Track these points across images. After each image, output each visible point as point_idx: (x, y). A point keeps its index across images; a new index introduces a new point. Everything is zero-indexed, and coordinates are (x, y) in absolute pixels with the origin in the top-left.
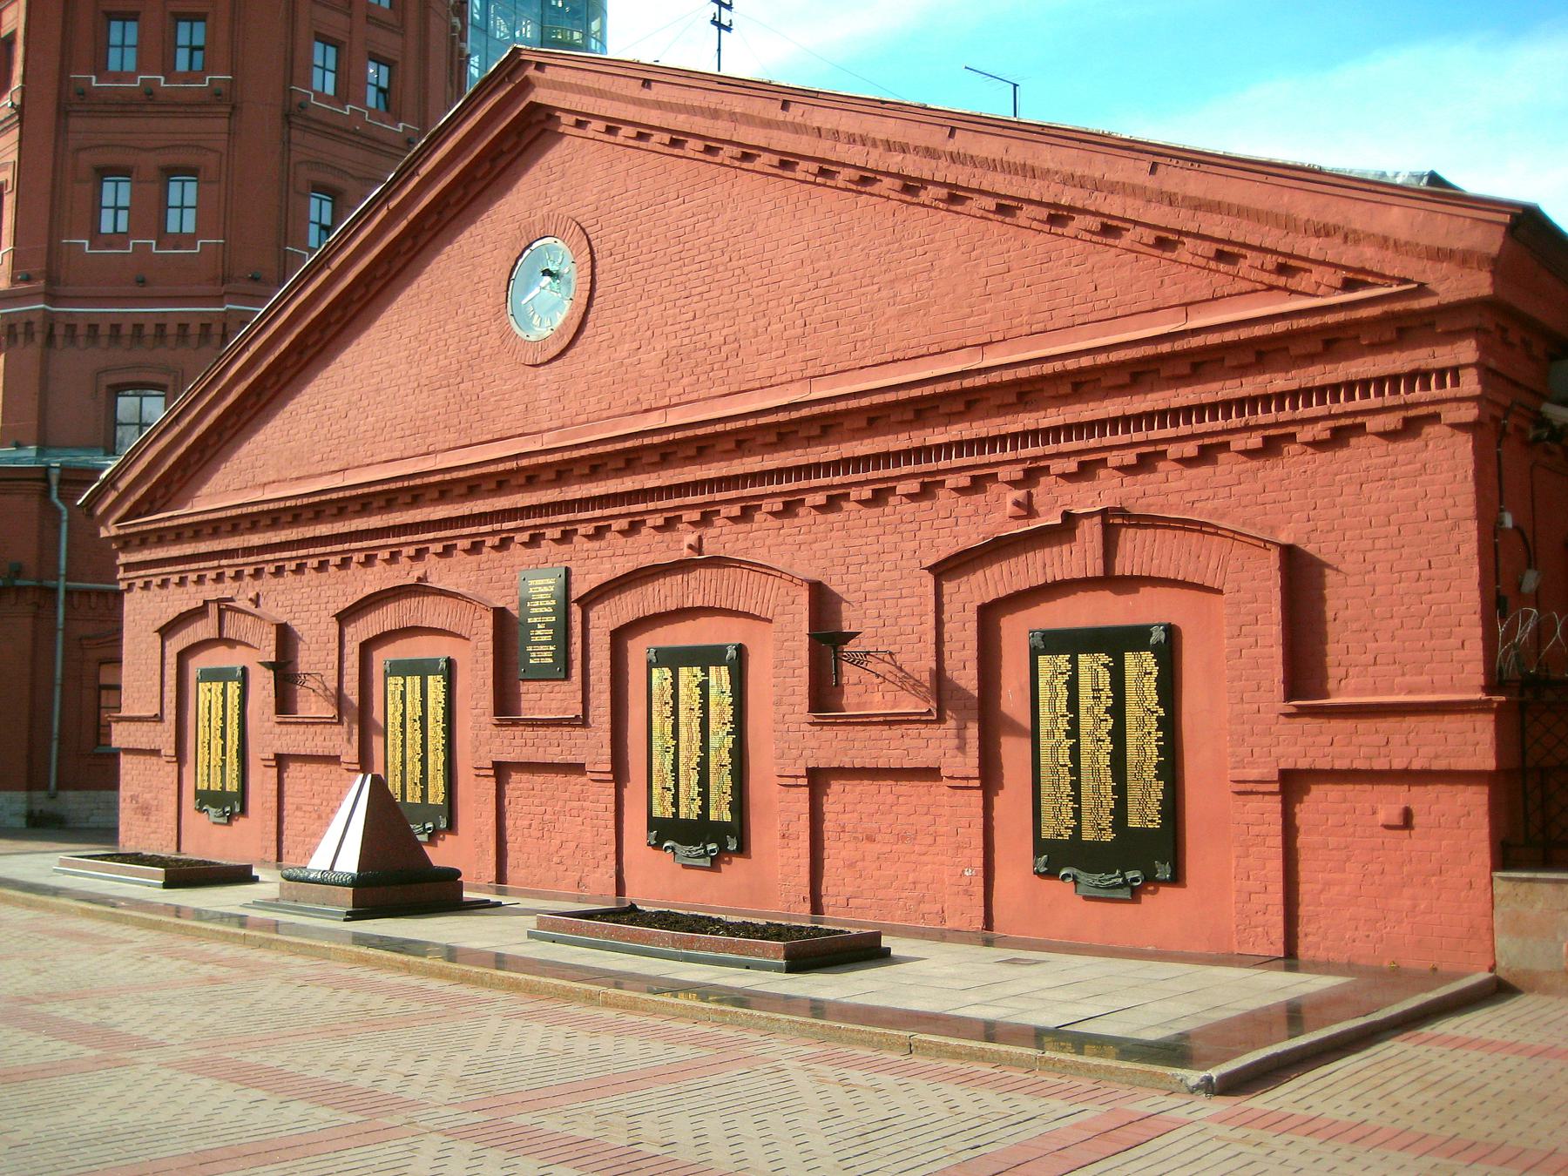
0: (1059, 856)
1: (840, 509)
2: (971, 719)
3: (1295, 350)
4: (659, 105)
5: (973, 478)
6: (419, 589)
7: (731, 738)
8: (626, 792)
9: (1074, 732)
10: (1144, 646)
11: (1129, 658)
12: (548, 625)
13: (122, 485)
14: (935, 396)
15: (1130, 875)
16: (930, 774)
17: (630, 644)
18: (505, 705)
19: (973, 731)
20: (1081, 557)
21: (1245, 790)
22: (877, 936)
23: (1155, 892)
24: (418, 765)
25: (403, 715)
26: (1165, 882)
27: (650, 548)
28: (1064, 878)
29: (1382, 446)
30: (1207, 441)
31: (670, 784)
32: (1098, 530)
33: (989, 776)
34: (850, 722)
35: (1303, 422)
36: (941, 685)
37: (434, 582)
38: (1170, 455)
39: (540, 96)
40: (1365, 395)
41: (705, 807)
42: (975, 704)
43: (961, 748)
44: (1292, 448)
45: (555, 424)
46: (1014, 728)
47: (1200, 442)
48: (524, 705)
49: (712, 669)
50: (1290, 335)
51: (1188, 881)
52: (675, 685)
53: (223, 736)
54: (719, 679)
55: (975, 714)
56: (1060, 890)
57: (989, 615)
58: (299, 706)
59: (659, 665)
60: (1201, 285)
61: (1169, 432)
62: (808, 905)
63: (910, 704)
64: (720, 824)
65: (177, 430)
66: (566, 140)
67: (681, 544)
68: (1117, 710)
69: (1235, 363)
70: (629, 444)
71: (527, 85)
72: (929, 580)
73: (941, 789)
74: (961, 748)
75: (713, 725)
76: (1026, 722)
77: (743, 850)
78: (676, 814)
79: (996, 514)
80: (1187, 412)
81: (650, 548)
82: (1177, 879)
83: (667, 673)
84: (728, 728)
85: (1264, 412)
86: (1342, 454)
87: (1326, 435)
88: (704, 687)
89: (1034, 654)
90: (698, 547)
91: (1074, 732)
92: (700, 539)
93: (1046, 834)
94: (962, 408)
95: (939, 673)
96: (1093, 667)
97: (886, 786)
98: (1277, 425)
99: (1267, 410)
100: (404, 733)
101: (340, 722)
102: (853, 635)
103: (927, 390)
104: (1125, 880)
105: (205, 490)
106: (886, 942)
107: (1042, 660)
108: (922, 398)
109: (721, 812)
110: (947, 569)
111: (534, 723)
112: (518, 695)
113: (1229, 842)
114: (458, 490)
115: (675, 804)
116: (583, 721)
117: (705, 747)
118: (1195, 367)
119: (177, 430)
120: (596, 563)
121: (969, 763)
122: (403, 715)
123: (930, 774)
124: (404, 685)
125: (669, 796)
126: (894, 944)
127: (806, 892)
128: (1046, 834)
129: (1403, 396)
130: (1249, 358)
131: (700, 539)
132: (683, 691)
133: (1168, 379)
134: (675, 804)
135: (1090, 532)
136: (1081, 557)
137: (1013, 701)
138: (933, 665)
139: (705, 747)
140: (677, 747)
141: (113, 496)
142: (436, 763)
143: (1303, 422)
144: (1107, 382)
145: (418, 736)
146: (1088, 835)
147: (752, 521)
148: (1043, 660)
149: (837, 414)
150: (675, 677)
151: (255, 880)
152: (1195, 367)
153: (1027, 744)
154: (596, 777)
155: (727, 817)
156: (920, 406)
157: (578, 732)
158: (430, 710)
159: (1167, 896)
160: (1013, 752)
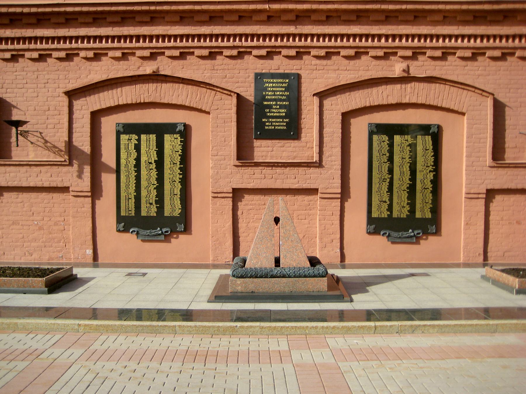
0: (127, 223)
1: (302, 59)
2: (87, 165)
3: (197, 18)
5: (12, 55)
6: (156, 77)
7: (432, 174)
8: (347, 204)
12: (281, 107)
15: (164, 230)
16: (65, 190)
17: (352, 121)
18: (244, 155)
19: (87, 170)
21: (217, 195)
22: (71, 269)
23: (177, 238)
25: (138, 160)
26: (181, 232)
27: (367, 68)
28: (132, 232)
29: (30, 63)
30: (125, 51)
31: (386, 198)
33: (96, 191)
34: (257, 164)
35: (28, 50)
36: (71, 149)
37: (413, 72)
38: (53, 56)
40: (59, 43)
41: (412, 211)
42: (89, 158)
43: (80, 176)
44: (281, 57)
46: (108, 169)
47: (327, 50)
48: (255, 154)
49: (419, 137)
50: (81, 13)
51: (192, 233)
55: (89, 161)
56: (380, 240)
57: (96, 116)
58: (13, 154)
59: (125, 133)
61: (26, 46)
62: (482, 258)
64: (172, 219)
67: (397, 68)
69: (83, 21)
70: (41, 10)
72: (66, 99)
73: (68, 197)
74: (80, 176)
75: (419, 167)
76: (113, 165)
77: (187, 230)
78: (390, 216)
80: (65, 39)
81: (367, 68)
84: (431, 168)
85: (112, 42)
86: (329, 62)
87: (148, 55)
90: (407, 70)
92: (408, 67)
94: (148, 19)
95: (70, 143)
96: (149, 141)
97: (33, 195)
98: (275, 47)
99: (83, 42)
101: (71, 164)
102: (25, 123)
104: (414, 234)
106: (75, 271)
107: (375, 137)
108: (15, 14)
109: (423, 212)
110: (73, 95)
112: (252, 148)
113: (209, 216)
115: (390, 208)
116: (319, 164)
118: (123, 19)
121: (85, 184)
122: (138, 160)
123: (65, 190)
124: (139, 140)
125: (385, 206)
126: (79, 272)
127: (482, 252)
128: (375, 215)
129: (267, 43)
130: (34, 21)
131: (408, 67)
133: (81, 23)
134: (390, 208)
137: (108, 156)
138: (67, 139)
140: (392, 179)
142: (172, 190)
143: (28, 50)
144: (284, 18)
147: (243, 58)
148: (375, 137)
149: (161, 12)
151: (83, 281)
152: (211, 18)
153: (114, 176)
154: (76, 194)
155: (429, 215)
156: (184, 15)
157: (317, 170)
159: (183, 237)
160: (108, 181)
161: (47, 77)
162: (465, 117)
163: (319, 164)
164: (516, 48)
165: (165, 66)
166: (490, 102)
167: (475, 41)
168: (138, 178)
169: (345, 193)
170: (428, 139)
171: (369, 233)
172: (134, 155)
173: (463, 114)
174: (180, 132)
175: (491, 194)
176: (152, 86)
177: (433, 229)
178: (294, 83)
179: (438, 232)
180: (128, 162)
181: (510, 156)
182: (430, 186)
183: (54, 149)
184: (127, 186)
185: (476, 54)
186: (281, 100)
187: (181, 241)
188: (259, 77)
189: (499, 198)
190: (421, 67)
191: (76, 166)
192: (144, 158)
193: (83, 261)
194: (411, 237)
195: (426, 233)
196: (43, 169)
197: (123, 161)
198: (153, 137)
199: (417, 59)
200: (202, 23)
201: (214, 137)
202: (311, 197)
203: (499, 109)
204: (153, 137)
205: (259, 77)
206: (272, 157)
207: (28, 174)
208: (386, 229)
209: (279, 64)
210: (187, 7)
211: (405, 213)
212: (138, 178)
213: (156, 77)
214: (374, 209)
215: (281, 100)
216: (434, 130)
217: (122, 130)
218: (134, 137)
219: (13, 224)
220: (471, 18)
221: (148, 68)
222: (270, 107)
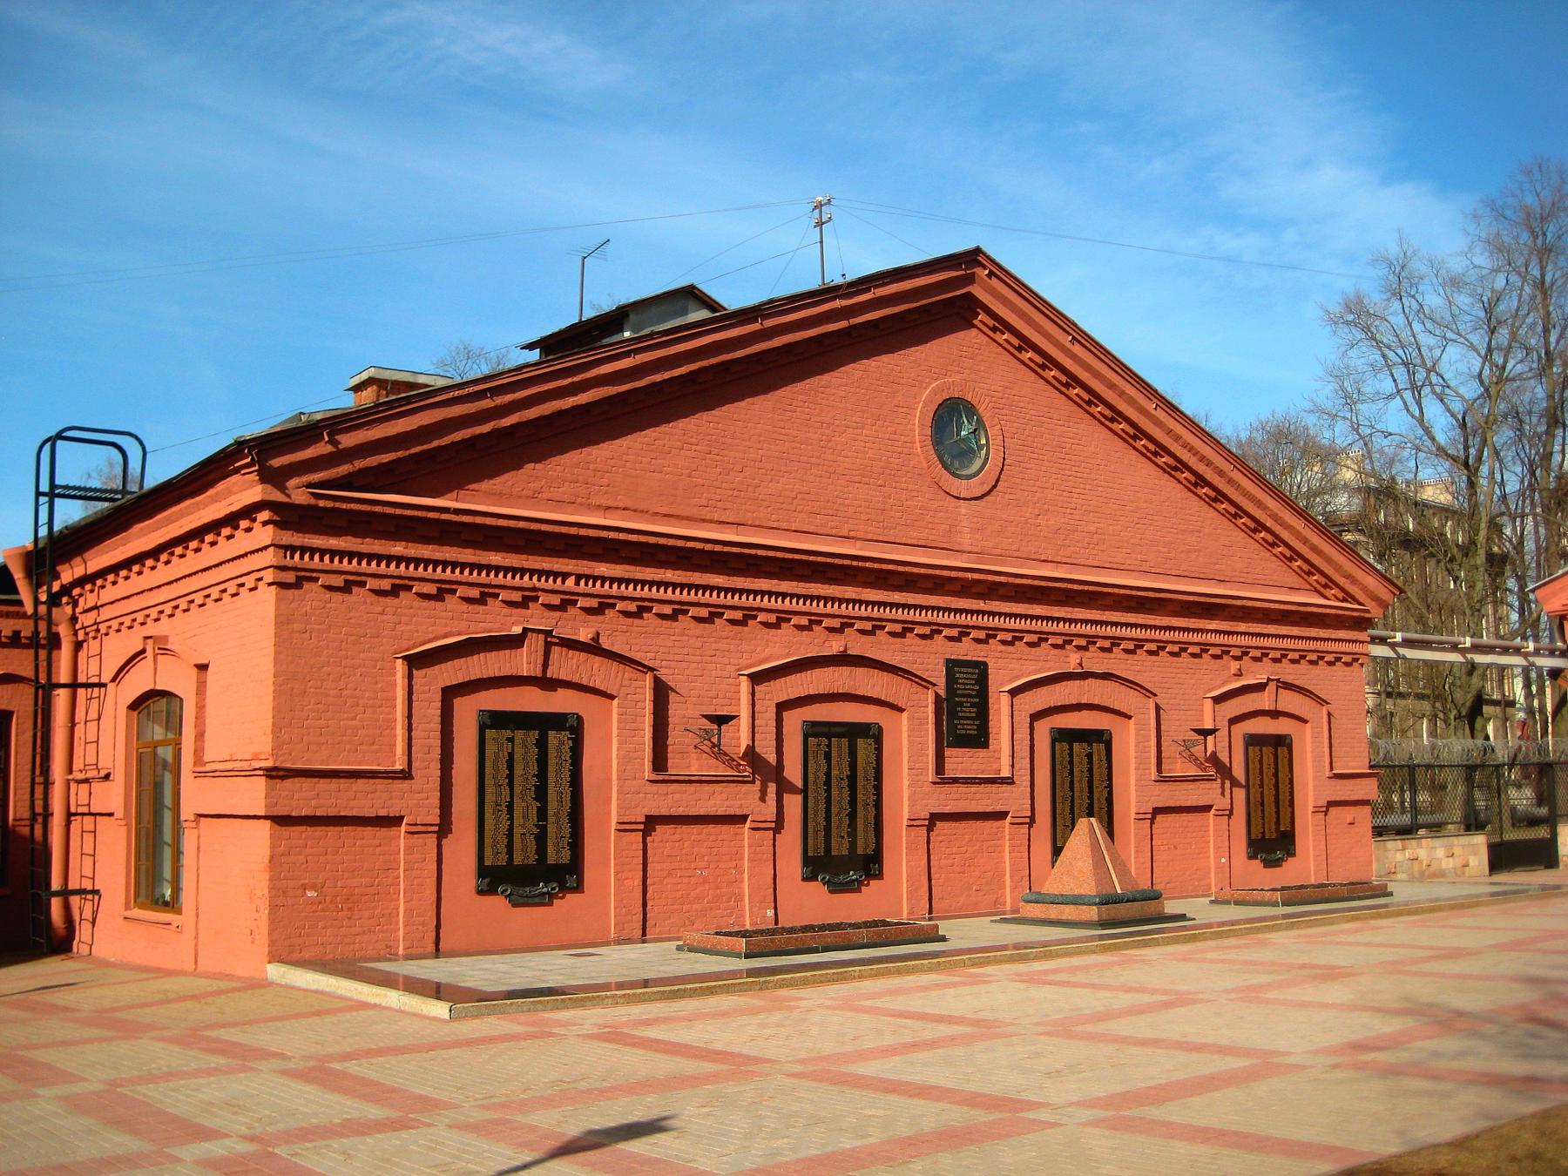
0: (492, 878)
4: (1074, 357)
8: (444, 842)
9: (1261, 786)
10: (867, 736)
11: (552, 734)
13: (348, 440)
14: (657, 545)
20: (524, 661)
24: (846, 820)
25: (828, 774)
27: (1072, 660)
32: (541, 643)
37: (605, 643)
39: (977, 291)
43: (763, 799)
44: (537, 605)
45: (975, 549)
46: (792, 789)
52: (1071, 755)
53: (541, 794)
54: (840, 748)
56: (497, 903)
59: (1059, 741)
60: (1295, 581)
63: (1193, 771)
65: (486, 403)
66: (974, 331)
68: (1276, 775)
71: (970, 279)
74: (763, 799)
75: (1096, 783)
76: (799, 784)
79: (451, 622)
81: (1072, 660)
82: (579, 888)
83: (1066, 746)
88: (1090, 756)
89: (482, 729)
91: (1261, 786)
93: (488, 863)
97: (332, 831)
98: (490, 586)
100: (828, 791)
103: (946, 573)
105: (485, 485)
111: (955, 781)
114: (1108, 602)
117: (1091, 797)
119: (486, 403)
120: (1047, 662)
122: (828, 774)
123: (1206, 809)
124: (829, 746)
128: (488, 863)
132: (1076, 759)
135: (535, 644)
136: (524, 661)
139: (1091, 797)
141: (321, 449)
145: (846, 792)
146: (518, 860)
148: (489, 733)
150: (1071, 748)
157: (1009, 787)
158: (860, 768)
159: (571, 898)
161: (714, 646)
162: (905, 715)
163: (406, 775)
164: (760, 610)
165: (882, 648)
166: (649, 677)
167: (434, 570)
168: (828, 800)
169: (444, 828)
170: (1102, 746)
171: (480, 892)
172: (824, 767)
173: (1130, 717)
174: (873, 736)
175: (651, 823)
176: (845, 671)
177: (571, 881)
178: (981, 669)
179: (579, 888)
180: (817, 777)
181: (675, 766)
182: (1105, 805)
183: (730, 761)
184: (816, 815)
185: (907, 629)
186: (970, 696)
187: (569, 903)
188: (952, 665)
189: (1159, 818)
190: (1116, 662)
191: (758, 783)
192: (834, 772)
193: (763, 927)
194: (543, 894)
195: (565, 889)
196: (717, 787)
197: (811, 778)
198: (845, 741)
199: (443, 600)
200: (426, 540)
201: (909, 742)
202: (999, 823)
203: (661, 692)
204: (845, 741)
205: (952, 665)
206: (309, 761)
207: (696, 796)
208: (824, 871)
209: (966, 650)
210: (890, 567)
211: (532, 859)
212: (828, 800)
213: (843, 659)
214: (488, 852)
215: (970, 696)
216: (572, 722)
217: (488, 722)
218: (825, 741)
219: (669, 875)
220: (1134, 604)
221: (835, 646)
222: (961, 704)
